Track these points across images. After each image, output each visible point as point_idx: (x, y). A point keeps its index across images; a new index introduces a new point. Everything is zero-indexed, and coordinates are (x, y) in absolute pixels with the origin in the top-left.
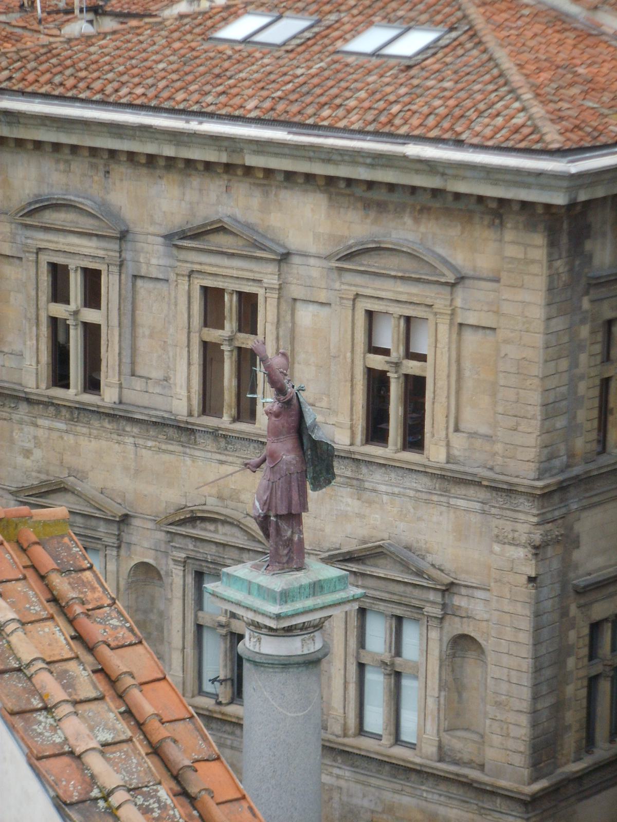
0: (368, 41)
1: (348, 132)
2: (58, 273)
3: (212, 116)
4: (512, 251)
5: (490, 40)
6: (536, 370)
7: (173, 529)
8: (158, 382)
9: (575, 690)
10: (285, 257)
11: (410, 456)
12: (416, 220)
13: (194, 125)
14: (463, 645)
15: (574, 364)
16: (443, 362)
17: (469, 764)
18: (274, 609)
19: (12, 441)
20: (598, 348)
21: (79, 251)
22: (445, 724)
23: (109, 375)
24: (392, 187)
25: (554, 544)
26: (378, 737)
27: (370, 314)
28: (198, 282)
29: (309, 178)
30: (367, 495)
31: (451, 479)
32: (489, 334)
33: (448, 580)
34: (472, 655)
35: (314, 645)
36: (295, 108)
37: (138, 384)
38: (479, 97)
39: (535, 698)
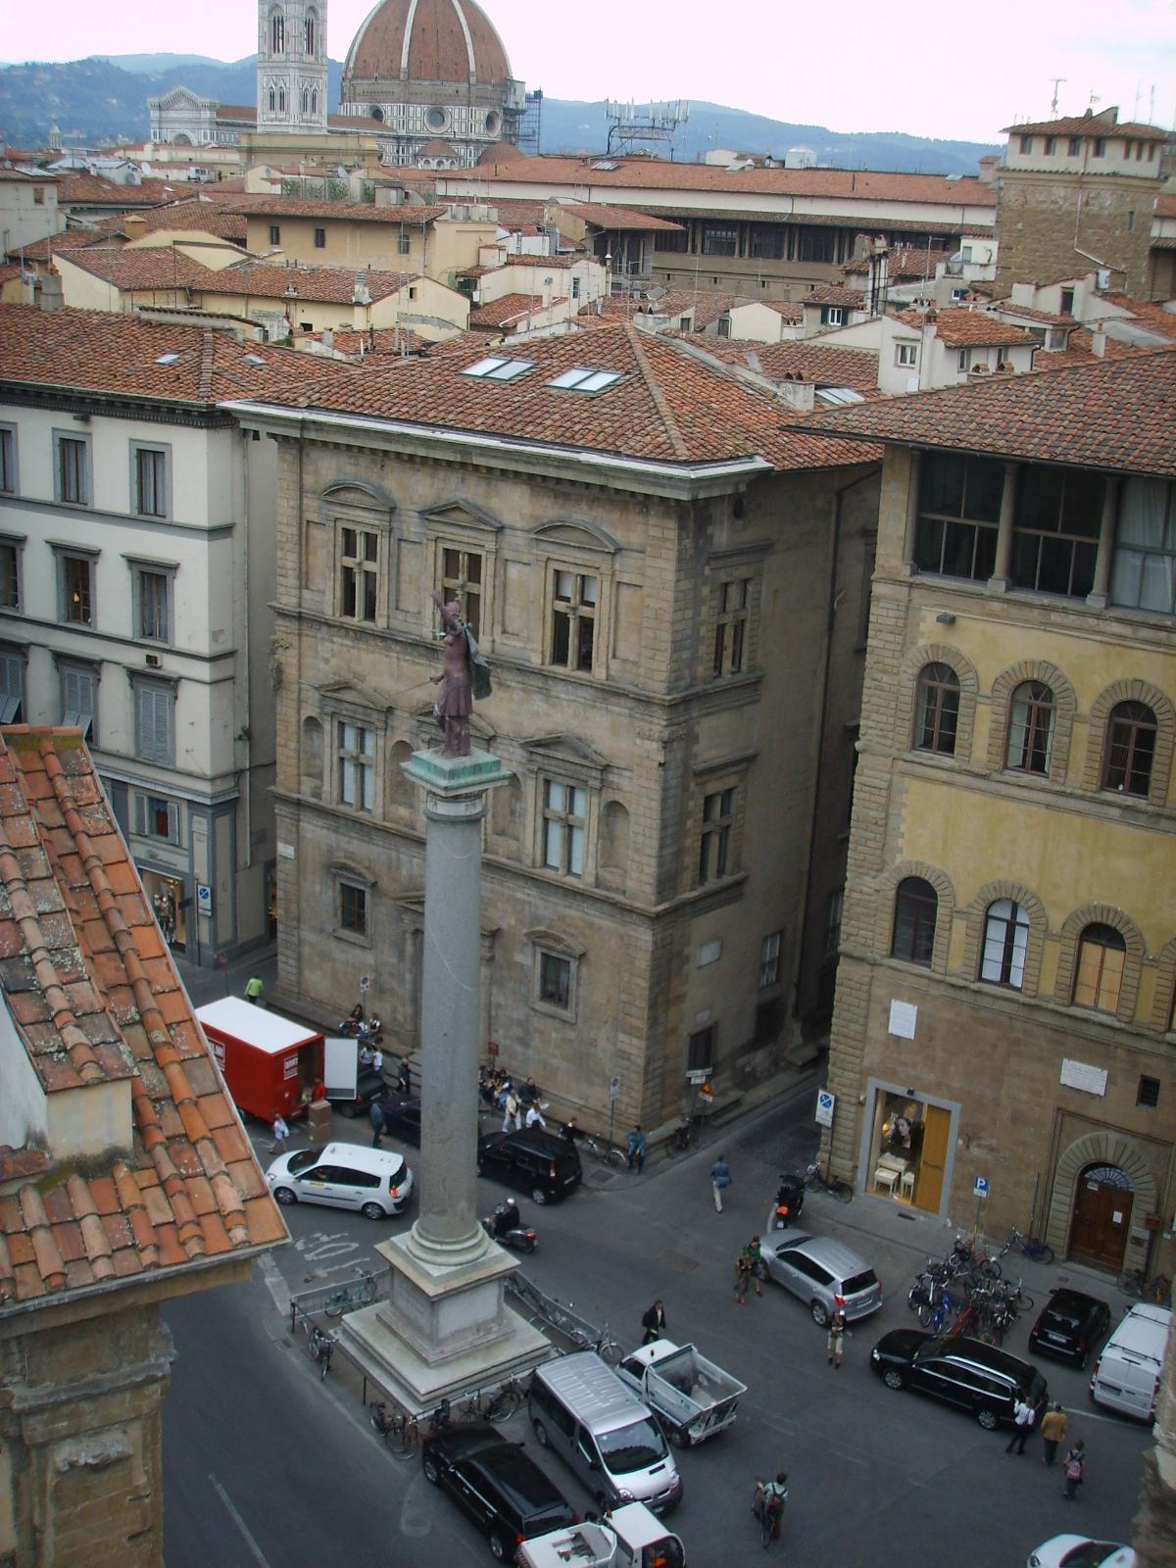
0: (566, 380)
1: (544, 443)
2: (349, 534)
3: (451, 428)
4: (654, 532)
5: (651, 382)
6: (668, 617)
7: (422, 718)
9: (692, 842)
10: (500, 530)
13: (438, 435)
14: (614, 808)
15: (697, 614)
17: (617, 890)
18: (444, 783)
19: (317, 653)
20: (715, 603)
21: (365, 520)
22: (601, 862)
23: (381, 609)
24: (573, 483)
25: (679, 741)
26: (556, 869)
27: (557, 573)
28: (441, 545)
29: (517, 474)
30: (553, 700)
31: (609, 692)
33: (605, 762)
35: (476, 808)
37: (401, 616)
38: (637, 421)
39: (662, 847)
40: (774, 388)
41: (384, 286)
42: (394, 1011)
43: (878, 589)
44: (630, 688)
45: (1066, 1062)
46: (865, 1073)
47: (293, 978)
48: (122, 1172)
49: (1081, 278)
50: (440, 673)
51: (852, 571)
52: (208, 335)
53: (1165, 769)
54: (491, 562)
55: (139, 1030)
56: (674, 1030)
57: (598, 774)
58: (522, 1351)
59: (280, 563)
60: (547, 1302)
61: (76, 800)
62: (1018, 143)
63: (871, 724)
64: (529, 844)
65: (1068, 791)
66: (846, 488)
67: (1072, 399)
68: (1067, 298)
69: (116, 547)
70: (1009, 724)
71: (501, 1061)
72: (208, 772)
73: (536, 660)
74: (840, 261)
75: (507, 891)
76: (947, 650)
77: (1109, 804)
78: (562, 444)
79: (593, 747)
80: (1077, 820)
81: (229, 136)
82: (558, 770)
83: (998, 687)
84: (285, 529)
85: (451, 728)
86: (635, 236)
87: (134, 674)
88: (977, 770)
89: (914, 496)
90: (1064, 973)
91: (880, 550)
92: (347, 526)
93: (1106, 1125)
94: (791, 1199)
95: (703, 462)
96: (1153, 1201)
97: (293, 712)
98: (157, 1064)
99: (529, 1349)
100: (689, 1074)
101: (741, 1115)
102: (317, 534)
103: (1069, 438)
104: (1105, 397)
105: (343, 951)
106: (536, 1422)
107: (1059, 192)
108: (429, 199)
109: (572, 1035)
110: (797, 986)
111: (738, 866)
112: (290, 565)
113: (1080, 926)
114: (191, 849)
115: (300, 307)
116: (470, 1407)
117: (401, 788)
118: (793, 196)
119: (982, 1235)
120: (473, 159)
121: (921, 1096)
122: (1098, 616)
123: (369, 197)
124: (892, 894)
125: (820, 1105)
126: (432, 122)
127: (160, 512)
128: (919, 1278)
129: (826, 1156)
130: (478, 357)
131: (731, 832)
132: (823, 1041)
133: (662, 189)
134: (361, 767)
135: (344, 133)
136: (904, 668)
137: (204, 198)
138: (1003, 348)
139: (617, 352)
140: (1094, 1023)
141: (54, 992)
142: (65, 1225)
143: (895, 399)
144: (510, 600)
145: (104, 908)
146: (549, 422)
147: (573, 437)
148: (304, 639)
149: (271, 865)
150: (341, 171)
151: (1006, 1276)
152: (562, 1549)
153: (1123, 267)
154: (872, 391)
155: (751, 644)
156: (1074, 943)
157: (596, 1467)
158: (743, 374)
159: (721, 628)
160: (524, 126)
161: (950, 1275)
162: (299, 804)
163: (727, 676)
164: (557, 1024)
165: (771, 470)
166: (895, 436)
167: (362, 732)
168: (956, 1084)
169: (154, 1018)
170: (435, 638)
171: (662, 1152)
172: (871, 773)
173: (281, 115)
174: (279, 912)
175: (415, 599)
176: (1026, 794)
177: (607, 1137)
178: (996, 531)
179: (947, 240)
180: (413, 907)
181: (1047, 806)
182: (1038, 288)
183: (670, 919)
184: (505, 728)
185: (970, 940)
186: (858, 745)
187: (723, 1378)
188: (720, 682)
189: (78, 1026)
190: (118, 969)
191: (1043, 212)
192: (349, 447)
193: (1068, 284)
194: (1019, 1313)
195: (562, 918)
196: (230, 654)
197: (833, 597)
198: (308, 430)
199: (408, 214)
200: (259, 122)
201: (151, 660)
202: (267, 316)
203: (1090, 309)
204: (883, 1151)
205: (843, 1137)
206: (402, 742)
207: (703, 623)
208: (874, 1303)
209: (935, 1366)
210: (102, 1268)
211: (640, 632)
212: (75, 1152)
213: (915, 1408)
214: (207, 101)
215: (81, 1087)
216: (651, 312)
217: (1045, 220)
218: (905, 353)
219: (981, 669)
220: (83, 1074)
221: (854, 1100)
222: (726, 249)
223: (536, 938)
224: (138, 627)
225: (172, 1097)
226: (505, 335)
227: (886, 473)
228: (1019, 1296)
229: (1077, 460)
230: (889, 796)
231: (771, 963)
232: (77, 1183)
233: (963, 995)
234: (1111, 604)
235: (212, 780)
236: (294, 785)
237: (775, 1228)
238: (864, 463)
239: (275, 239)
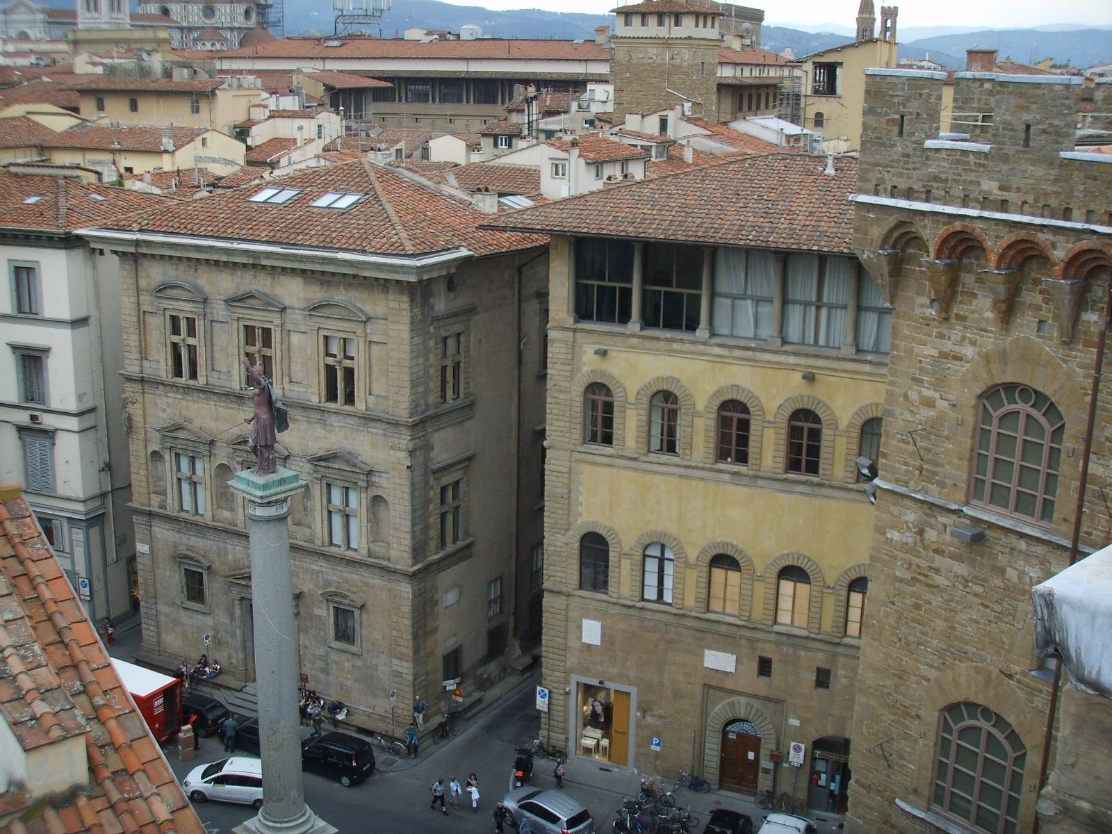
0: (324, 201)
1: (311, 247)
2: (175, 320)
3: (244, 240)
4: (393, 304)
5: (384, 199)
6: (407, 363)
7: (235, 447)
8: (225, 373)
9: (434, 520)
10: (283, 310)
11: (348, 408)
12: (346, 290)
13: (235, 245)
14: (377, 500)
15: (427, 360)
16: (362, 360)
17: (383, 558)
18: (260, 493)
19: (156, 405)
20: (439, 351)
21: (185, 309)
22: (371, 539)
23: (201, 371)
24: (333, 274)
25: (420, 449)
26: (340, 546)
27: (326, 338)
28: (242, 323)
29: (293, 270)
30: (328, 428)
31: (369, 419)
32: (384, 347)
33: (369, 469)
34: (383, 505)
35: (284, 510)
36: (285, 235)
37: (215, 374)
38: (376, 228)
39: (413, 525)
40: (469, 199)
41: (184, 137)
42: (230, 657)
43: (552, 334)
44: (383, 415)
45: (707, 651)
46: (568, 672)
47: (155, 640)
48: (82, 801)
49: (672, 109)
50: (251, 416)
51: (531, 322)
52: (62, 182)
53: (759, 445)
55: (84, 698)
56: (432, 653)
59: (125, 342)
61: (21, 536)
62: (622, 19)
63: (553, 428)
65: (694, 464)
66: (525, 264)
67: (676, 196)
68: (664, 124)
71: (310, 686)
72: (81, 496)
73: (315, 400)
74: (503, 103)
75: (305, 565)
76: (603, 374)
77: (721, 471)
78: (324, 247)
80: (701, 484)
81: (58, 32)
82: (335, 476)
83: (640, 396)
84: (127, 318)
85: (261, 453)
86: (359, 92)
87: (21, 429)
88: (630, 455)
89: (572, 268)
91: (552, 307)
93: (738, 693)
94: (524, 765)
96: (774, 742)
97: (142, 449)
98: (99, 720)
103: (676, 223)
104: (699, 193)
105: (190, 617)
107: (653, 51)
108: (211, 74)
109: (359, 663)
111: (467, 534)
112: (133, 344)
113: (709, 557)
114: (72, 553)
115: (123, 155)
117: (224, 497)
118: (467, 59)
119: (659, 778)
120: (237, 41)
121: (608, 684)
122: (705, 343)
123: (168, 74)
124: (577, 546)
125: (538, 697)
126: (206, 16)
127: (34, 311)
128: (619, 812)
129: (545, 733)
130: (259, 188)
131: (461, 511)
132: (535, 652)
133: (375, 58)
134: (194, 484)
135: (142, 26)
136: (573, 388)
137: (46, 79)
138: (624, 162)
139: (357, 180)
140: (724, 623)
143: (555, 203)
144: (293, 359)
145: (50, 612)
146: (313, 232)
148: (146, 395)
149: (132, 559)
150: (145, 56)
151: (678, 804)
153: (699, 100)
154: (537, 197)
156: (705, 570)
158: (447, 190)
159: (444, 369)
160: (272, 16)
161: (640, 808)
162: (150, 514)
163: (450, 402)
164: (349, 656)
165: (472, 256)
167: (193, 459)
168: (632, 674)
169: (93, 688)
170: (241, 389)
171: (431, 741)
172: (557, 462)
173: (95, 15)
174: (140, 593)
175: (226, 362)
176: (664, 469)
177: (390, 734)
178: (631, 289)
179: (576, 85)
180: (239, 582)
181: (681, 476)
182: (643, 116)
183: (423, 576)
184: (296, 449)
185: (634, 573)
186: (545, 444)
189: (43, 700)
190: (64, 655)
191: (643, 65)
192: (171, 257)
193: (664, 113)
194: (690, 830)
195: (346, 581)
196: (92, 410)
197: (520, 340)
198: (141, 246)
199: (197, 85)
200: (80, 20)
201: (33, 418)
202: (99, 163)
203: (680, 130)
204: (585, 726)
205: (557, 718)
211: (387, 376)
214: (39, 6)
216: (379, 150)
217: (645, 70)
218: (558, 169)
219: (627, 385)
220: (50, 734)
221: (562, 692)
222: (423, 98)
223: (329, 597)
224: (23, 395)
225: (112, 744)
226: (273, 168)
227: (552, 254)
228: (689, 817)
229: (683, 238)
230: (570, 478)
231: (495, 600)
232: (50, 814)
233: (632, 612)
234: (713, 334)
235: (84, 501)
236: (146, 501)
237: (515, 787)
238: (536, 247)
239: (101, 107)
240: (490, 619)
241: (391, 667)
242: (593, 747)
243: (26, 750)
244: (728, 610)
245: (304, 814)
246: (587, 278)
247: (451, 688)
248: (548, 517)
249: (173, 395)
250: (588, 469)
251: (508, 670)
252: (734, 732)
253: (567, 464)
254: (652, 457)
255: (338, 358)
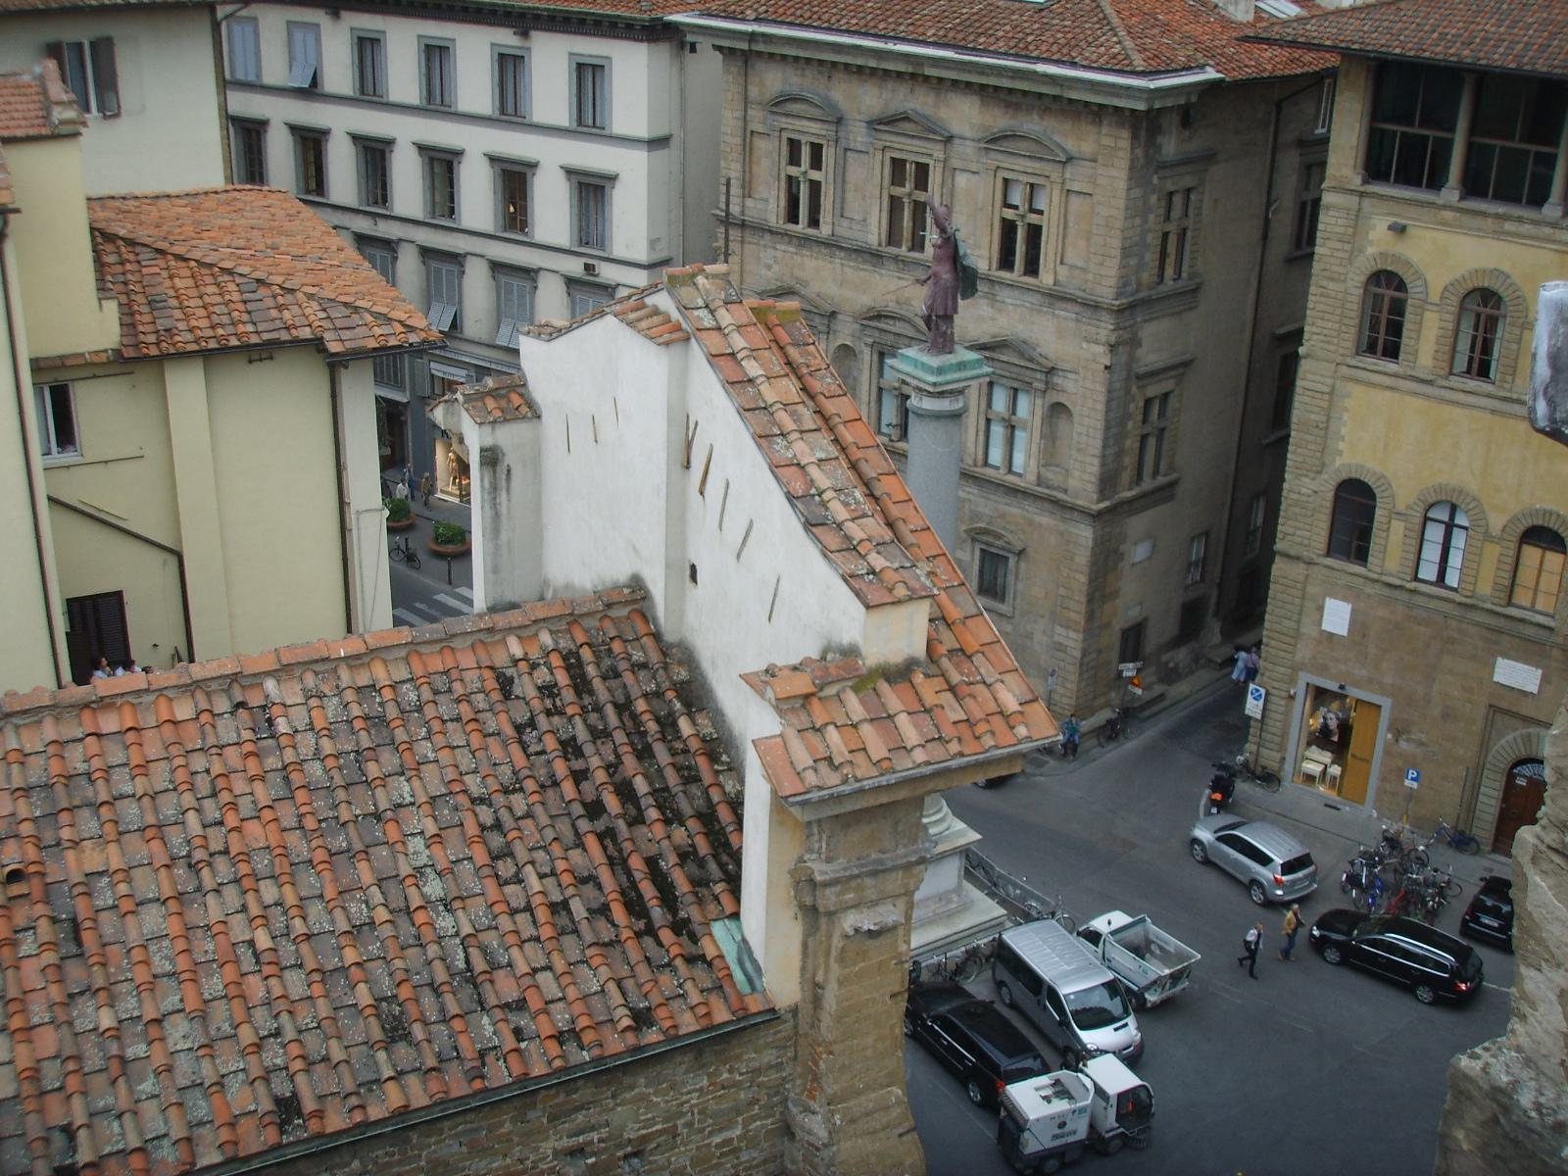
1: (996, 54)
4: (1107, 141)
6: (1118, 224)
7: (865, 322)
8: (859, 222)
9: (1131, 443)
10: (949, 139)
12: (1041, 118)
13: (890, 46)
14: (1058, 409)
15: (1145, 221)
16: (1055, 216)
18: (932, 379)
19: (759, 258)
20: (1162, 211)
21: (810, 130)
22: (1042, 462)
24: (1025, 93)
25: (1124, 344)
26: (997, 468)
27: (1006, 181)
28: (889, 154)
29: (968, 85)
31: (1056, 297)
32: (1088, 199)
33: (1050, 365)
36: (960, 36)
37: (845, 223)
39: (1105, 447)
43: (1328, 198)
45: (1500, 660)
46: (1295, 669)
48: (918, 678)
54: (939, 170)
56: (1108, 625)
57: (1043, 377)
58: (977, 922)
60: (1000, 876)
64: (971, 445)
65: (1515, 396)
69: (553, 160)
70: (1457, 332)
76: (1396, 258)
79: (1039, 350)
85: (937, 325)
87: (571, 282)
90: (1503, 574)
92: (793, 136)
95: (1159, 72)
99: (987, 918)
100: (1122, 666)
101: (1165, 709)
102: (761, 144)
106: (1000, 984)
110: (1219, 585)
111: (1171, 468)
113: (1521, 528)
116: (938, 969)
122: (1554, 225)
124: (1330, 495)
125: (1250, 698)
127: (598, 124)
128: (1352, 863)
129: (1254, 748)
131: (1166, 435)
136: (1351, 275)
140: (1531, 623)
141: (849, 524)
142: (884, 720)
146: (1000, 34)
147: (1026, 48)
148: (746, 246)
152: (1044, 1093)
155: (1192, 252)
156: (1513, 546)
157: (1064, 1023)
159: (1166, 235)
161: (1381, 862)
165: (1222, 80)
166: (1356, 46)
168: (1388, 680)
171: (1094, 741)
176: (1471, 399)
181: (1493, 412)
183: (1109, 518)
185: (1408, 541)
187: (1177, 947)
188: (1162, 289)
192: (796, 59)
195: (1002, 516)
197: (1269, 204)
198: (757, 42)
201: (589, 268)
204: (1309, 744)
206: (844, 346)
207: (1149, 231)
208: (1310, 885)
209: (1374, 943)
210: (920, 756)
212: (881, 660)
213: (1350, 979)
215: (893, 603)
219: (1429, 277)
220: (895, 592)
221: (1285, 694)
224: (576, 237)
227: (1341, 82)
228: (1449, 882)
229: (1545, 69)
230: (1331, 401)
231: (1196, 564)
232: (884, 686)
233: (1397, 594)
237: (1208, 813)
240: (1187, 588)
241: (1052, 637)
242: (1317, 775)
243: (868, 607)
244: (1539, 607)
245: (940, 810)
246: (1386, 121)
247: (1130, 674)
248: (1294, 453)
249: (783, 247)
250: (1358, 391)
251: (1202, 662)
252: (1525, 776)
253: (1329, 381)
254: (1455, 381)
255: (1021, 210)
